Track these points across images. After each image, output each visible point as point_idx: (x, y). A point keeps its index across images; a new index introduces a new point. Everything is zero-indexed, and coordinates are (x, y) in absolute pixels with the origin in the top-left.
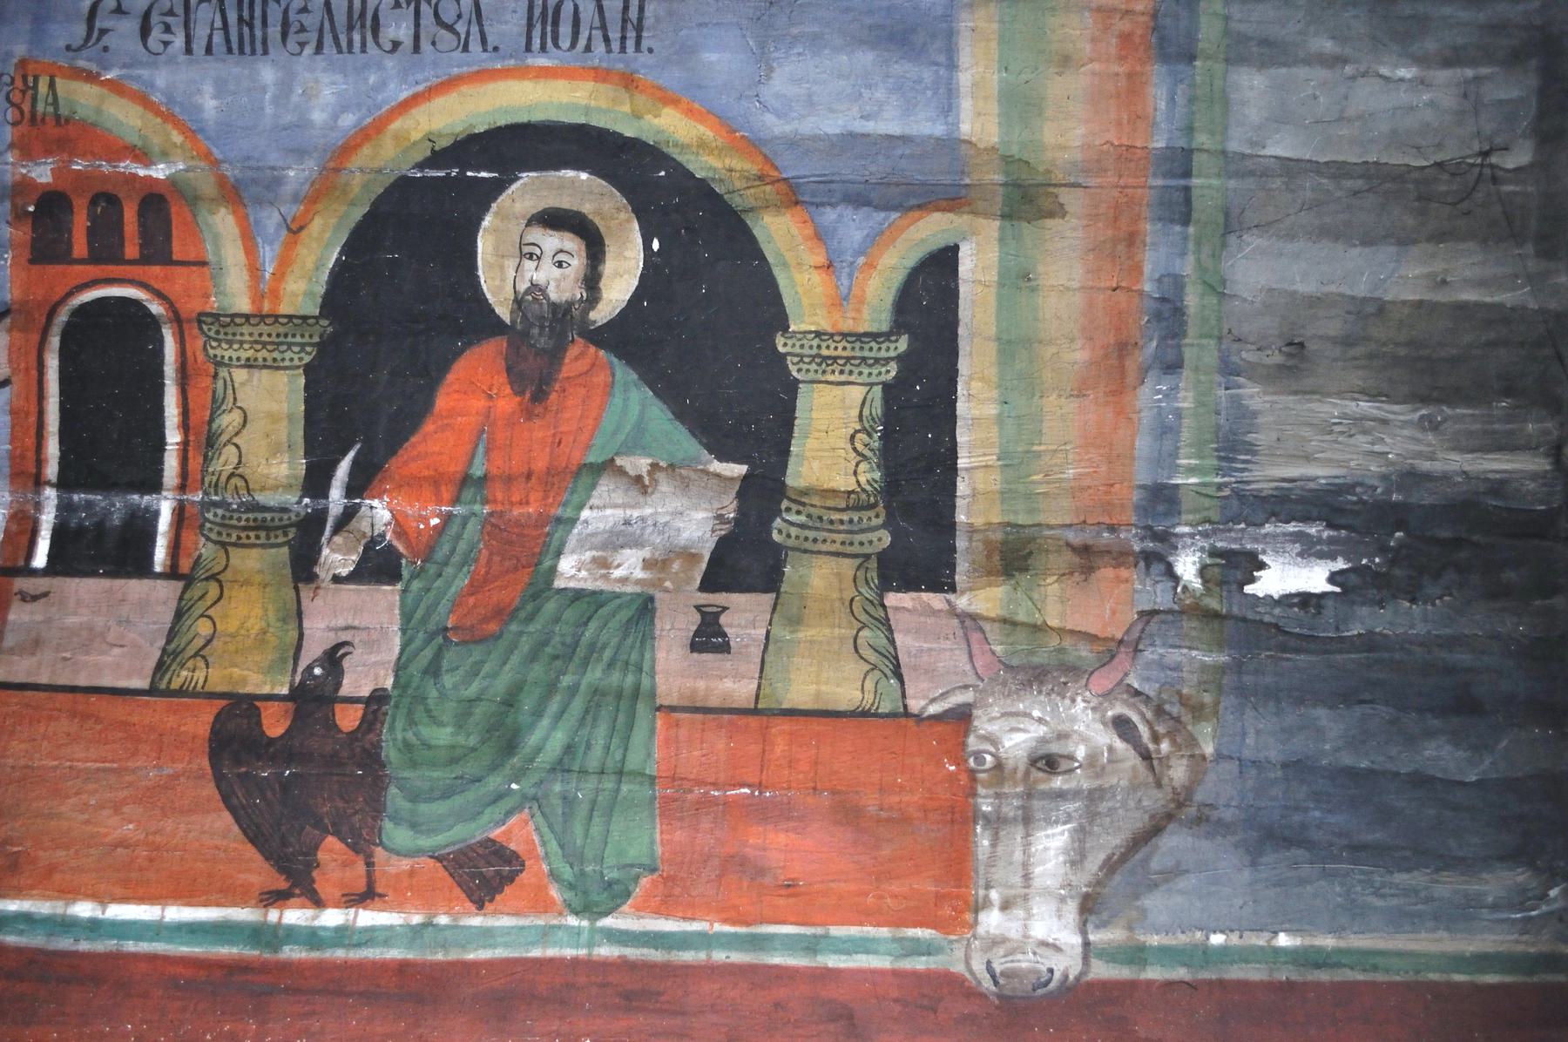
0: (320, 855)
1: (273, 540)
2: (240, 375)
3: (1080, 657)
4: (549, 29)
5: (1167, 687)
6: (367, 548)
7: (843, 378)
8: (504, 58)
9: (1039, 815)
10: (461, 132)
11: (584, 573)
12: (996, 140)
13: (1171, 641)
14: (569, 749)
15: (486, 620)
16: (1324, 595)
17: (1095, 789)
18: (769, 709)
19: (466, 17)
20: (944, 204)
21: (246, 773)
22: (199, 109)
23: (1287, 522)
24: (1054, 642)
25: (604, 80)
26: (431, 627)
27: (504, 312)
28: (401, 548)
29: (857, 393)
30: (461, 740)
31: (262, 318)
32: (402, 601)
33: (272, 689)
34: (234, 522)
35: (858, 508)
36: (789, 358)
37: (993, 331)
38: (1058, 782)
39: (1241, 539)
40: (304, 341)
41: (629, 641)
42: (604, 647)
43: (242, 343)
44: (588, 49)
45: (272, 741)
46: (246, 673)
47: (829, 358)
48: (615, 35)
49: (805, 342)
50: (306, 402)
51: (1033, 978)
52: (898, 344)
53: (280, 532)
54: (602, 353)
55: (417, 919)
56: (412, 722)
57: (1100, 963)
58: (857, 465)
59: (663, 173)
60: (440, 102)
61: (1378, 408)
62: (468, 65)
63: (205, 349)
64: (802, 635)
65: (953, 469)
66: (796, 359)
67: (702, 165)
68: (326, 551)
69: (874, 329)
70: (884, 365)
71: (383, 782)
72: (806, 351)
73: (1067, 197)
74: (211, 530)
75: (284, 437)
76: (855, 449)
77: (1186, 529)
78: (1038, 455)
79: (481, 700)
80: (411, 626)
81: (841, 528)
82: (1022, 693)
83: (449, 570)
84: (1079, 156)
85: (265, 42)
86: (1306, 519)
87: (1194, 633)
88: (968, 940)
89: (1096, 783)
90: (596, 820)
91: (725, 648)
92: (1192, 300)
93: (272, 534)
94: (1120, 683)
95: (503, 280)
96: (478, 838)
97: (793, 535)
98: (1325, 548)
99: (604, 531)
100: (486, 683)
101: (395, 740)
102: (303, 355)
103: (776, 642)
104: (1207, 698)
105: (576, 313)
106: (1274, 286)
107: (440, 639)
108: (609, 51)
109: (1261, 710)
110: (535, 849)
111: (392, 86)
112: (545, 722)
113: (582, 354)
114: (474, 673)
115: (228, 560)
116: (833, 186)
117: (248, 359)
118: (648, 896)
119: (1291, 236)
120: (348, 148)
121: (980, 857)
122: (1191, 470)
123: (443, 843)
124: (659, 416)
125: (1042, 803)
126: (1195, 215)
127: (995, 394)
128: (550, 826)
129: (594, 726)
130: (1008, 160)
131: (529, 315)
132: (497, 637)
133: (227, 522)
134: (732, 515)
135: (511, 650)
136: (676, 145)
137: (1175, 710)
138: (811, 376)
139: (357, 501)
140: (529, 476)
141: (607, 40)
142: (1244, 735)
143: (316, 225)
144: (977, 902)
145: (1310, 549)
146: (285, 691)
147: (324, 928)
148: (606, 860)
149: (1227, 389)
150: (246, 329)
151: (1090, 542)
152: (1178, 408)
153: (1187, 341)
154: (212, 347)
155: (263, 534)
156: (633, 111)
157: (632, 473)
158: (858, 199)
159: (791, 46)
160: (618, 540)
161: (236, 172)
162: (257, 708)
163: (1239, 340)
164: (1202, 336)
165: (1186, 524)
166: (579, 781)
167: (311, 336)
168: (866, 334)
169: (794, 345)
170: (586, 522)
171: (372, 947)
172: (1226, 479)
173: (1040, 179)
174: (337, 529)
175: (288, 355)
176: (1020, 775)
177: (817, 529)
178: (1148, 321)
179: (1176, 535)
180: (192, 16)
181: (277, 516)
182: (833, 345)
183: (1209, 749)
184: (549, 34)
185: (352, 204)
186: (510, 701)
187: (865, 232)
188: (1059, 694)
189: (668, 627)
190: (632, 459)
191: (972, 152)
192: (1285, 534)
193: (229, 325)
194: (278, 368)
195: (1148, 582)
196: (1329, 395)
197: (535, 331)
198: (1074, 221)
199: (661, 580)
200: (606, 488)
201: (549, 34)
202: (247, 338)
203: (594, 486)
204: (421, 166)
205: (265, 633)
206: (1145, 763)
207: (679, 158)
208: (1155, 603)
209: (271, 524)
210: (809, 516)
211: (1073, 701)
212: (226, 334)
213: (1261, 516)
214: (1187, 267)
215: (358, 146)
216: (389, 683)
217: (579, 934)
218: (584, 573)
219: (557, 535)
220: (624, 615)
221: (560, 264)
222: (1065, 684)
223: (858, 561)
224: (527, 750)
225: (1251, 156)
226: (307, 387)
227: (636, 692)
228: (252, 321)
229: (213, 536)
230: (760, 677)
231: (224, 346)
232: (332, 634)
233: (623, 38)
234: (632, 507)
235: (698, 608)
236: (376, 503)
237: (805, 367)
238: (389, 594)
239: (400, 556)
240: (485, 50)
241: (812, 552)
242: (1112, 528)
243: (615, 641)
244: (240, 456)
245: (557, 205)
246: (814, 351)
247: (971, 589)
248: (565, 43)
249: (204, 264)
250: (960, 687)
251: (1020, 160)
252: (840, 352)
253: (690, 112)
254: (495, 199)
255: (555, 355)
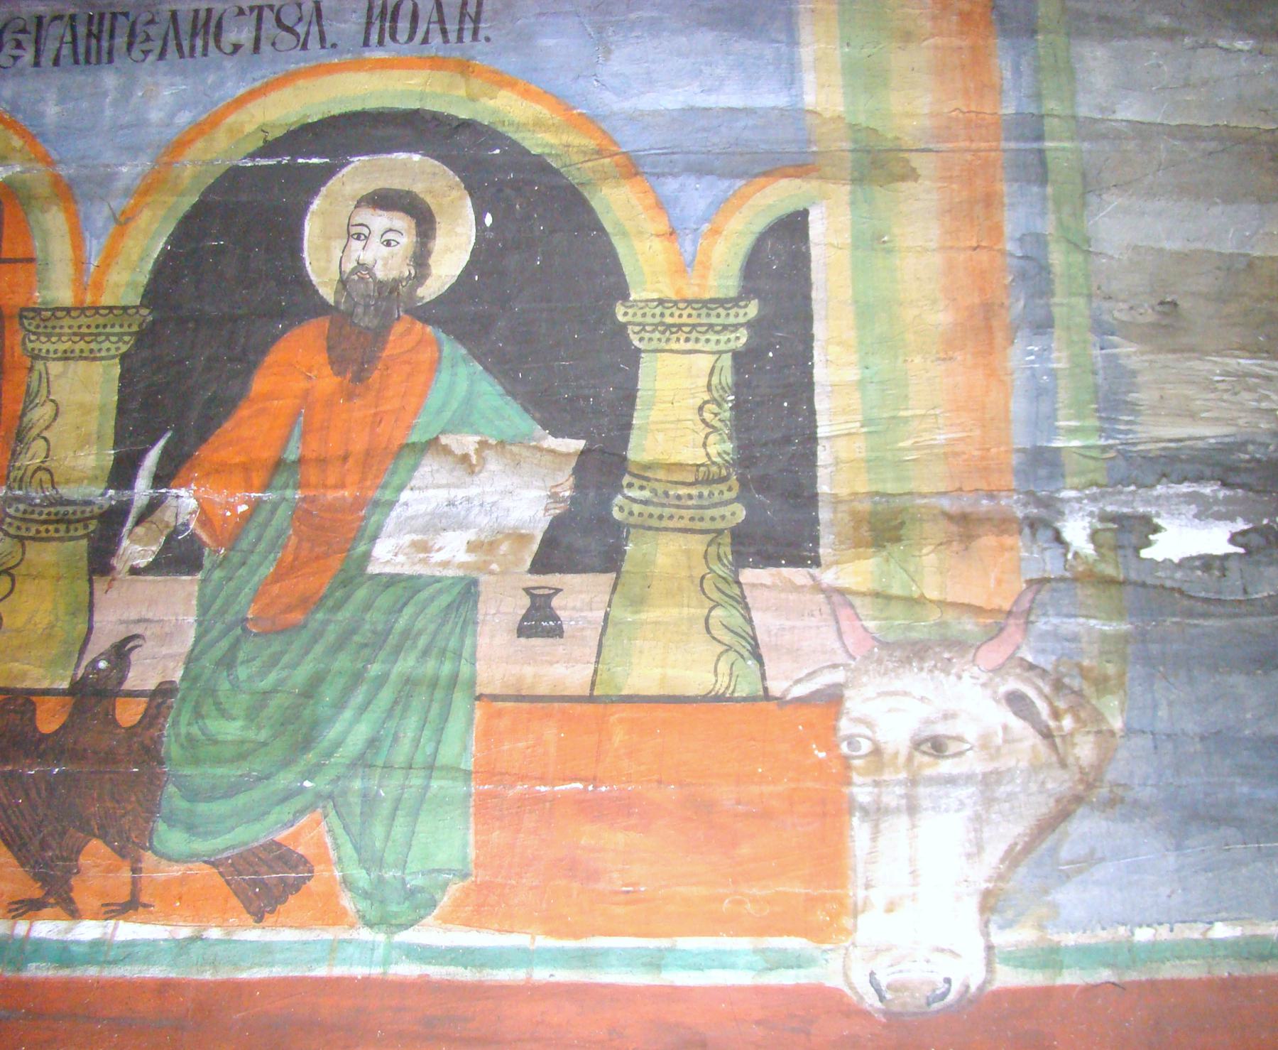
0: (83, 860)
1: (72, 533)
2: (55, 368)
3: (965, 631)
4: (387, 24)
5: (1065, 659)
6: (170, 538)
7: (690, 346)
8: (341, 53)
9: (925, 803)
10: (295, 122)
11: (401, 558)
12: (842, 109)
13: (1065, 610)
14: (373, 743)
15: (289, 609)
16: (1226, 557)
17: (991, 773)
18: (607, 696)
19: (306, 19)
20: (791, 171)
21: (11, 771)
22: (42, 115)
23: (1180, 482)
24: (934, 615)
25: (440, 68)
26: (229, 617)
27: (328, 293)
28: (205, 537)
29: (705, 362)
30: (251, 734)
31: (82, 310)
32: (201, 590)
33: (52, 683)
34: (35, 516)
35: (709, 481)
36: (630, 327)
37: (848, 294)
38: (946, 767)
39: (1133, 501)
40: (122, 330)
41: (447, 628)
42: (419, 634)
43: (60, 335)
44: (425, 41)
45: (44, 737)
46: (27, 667)
47: (673, 325)
48: (452, 27)
49: (647, 310)
50: (120, 391)
51: (927, 990)
52: (747, 310)
53: (80, 526)
54: (429, 329)
55: (184, 932)
56: (198, 715)
57: (1007, 969)
58: (706, 437)
59: (497, 151)
60: (274, 96)
61: (1260, 365)
62: (306, 61)
63: (24, 344)
64: (650, 615)
65: (812, 439)
66: (637, 329)
67: (537, 143)
68: (125, 543)
69: (721, 295)
70: (732, 332)
71: (159, 779)
72: (649, 320)
73: (917, 161)
74: (10, 524)
75: (94, 427)
76: (704, 421)
77: (1073, 494)
78: (906, 420)
79: (277, 692)
80: (208, 617)
81: (690, 503)
82: (901, 670)
83: (254, 559)
84: (927, 123)
85: (110, 52)
86: (1199, 479)
87: (1090, 602)
88: (847, 949)
89: (990, 766)
90: (400, 819)
91: (557, 632)
92: (1057, 257)
93: (72, 527)
94: (1011, 657)
95: (329, 261)
96: (262, 841)
97: (636, 513)
98: (1223, 509)
99: (426, 514)
100: (285, 673)
101: (178, 735)
102: (120, 344)
103: (616, 624)
104: (1111, 669)
105: (402, 289)
106: (1140, 244)
107: (239, 631)
108: (446, 41)
109: (1172, 680)
110: (327, 853)
111: (230, 84)
112: (348, 714)
113: (408, 332)
114: (274, 662)
115: (24, 553)
116: (675, 157)
117: (65, 352)
118: (458, 904)
119: (1151, 194)
120: (181, 144)
121: (858, 853)
122: (1072, 432)
123: (221, 847)
124: (489, 392)
125: (928, 790)
126: (1051, 176)
127: (855, 358)
128: (346, 827)
129: (402, 718)
130: (854, 127)
131: (354, 294)
132: (298, 628)
133: (27, 516)
134: (567, 493)
135: (315, 639)
136: (511, 124)
137: (1076, 683)
138: (654, 345)
139: (163, 491)
140: (345, 458)
141: (444, 32)
142: (1155, 707)
143: (145, 217)
144: (855, 904)
145: (1206, 510)
146: (65, 685)
147: (78, 943)
148: (408, 865)
149: (1102, 349)
150: (67, 322)
151: (968, 510)
152: (1053, 369)
153: (1056, 300)
154: (31, 341)
155: (62, 527)
156: (468, 95)
157: (459, 452)
158: (700, 170)
159: (631, 29)
160: (438, 523)
161: (71, 171)
162: (33, 703)
163: (1110, 298)
164: (1071, 294)
165: (1072, 488)
166: (382, 777)
167: (130, 326)
168: (713, 301)
169: (635, 315)
170: (406, 504)
171: (131, 964)
172: (1111, 442)
173: (889, 145)
174: (139, 522)
175: (106, 345)
176: (902, 759)
177: (663, 505)
178: (1013, 280)
179: (1062, 500)
180: (44, 33)
181: (79, 509)
182: (677, 313)
183: (1117, 723)
184: (387, 29)
185: (182, 194)
186: (310, 691)
187: (709, 200)
188: (943, 670)
189: (493, 611)
190: (458, 437)
191: (817, 122)
192: (1178, 496)
193: (49, 319)
194: (95, 359)
195: (1035, 549)
196: (1208, 354)
197: (360, 310)
198: (928, 183)
199: (487, 563)
200: (429, 468)
201: (387, 29)
202: (66, 330)
203: (415, 467)
204: (252, 156)
205: (53, 626)
206: (1045, 742)
207: (516, 136)
208: (1044, 570)
209: (73, 517)
210: (654, 491)
211: (959, 677)
212: (46, 327)
213: (1150, 479)
214: (1048, 226)
215: (192, 141)
216: (177, 676)
217: (373, 950)
218: (401, 558)
219: (373, 519)
220: (444, 600)
221: (388, 243)
222: (949, 660)
223: (709, 537)
224: (325, 744)
225: (1103, 120)
226: (122, 377)
227: (454, 680)
228: (73, 314)
229: (12, 531)
230: (597, 662)
231: (43, 339)
232: (122, 628)
233: (461, 30)
234: (457, 487)
235: (527, 590)
236: (182, 492)
237: (647, 336)
238: (187, 587)
239: (203, 544)
240: (323, 47)
241: (657, 529)
242: (991, 495)
243: (432, 627)
244: (48, 450)
245: (387, 186)
246: (657, 320)
247: (837, 563)
248: (402, 36)
249: (31, 260)
250: (828, 667)
251: (868, 128)
252: (685, 320)
253: (526, 94)
254: (324, 184)
255: (379, 335)
